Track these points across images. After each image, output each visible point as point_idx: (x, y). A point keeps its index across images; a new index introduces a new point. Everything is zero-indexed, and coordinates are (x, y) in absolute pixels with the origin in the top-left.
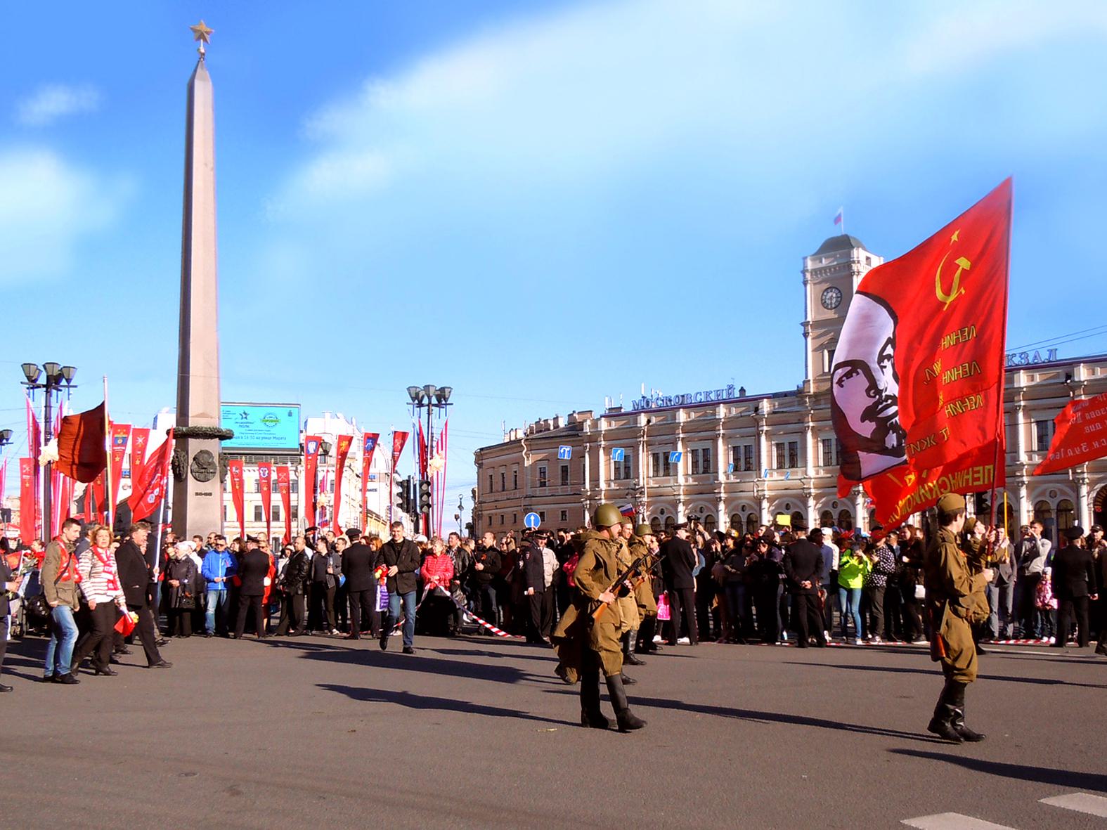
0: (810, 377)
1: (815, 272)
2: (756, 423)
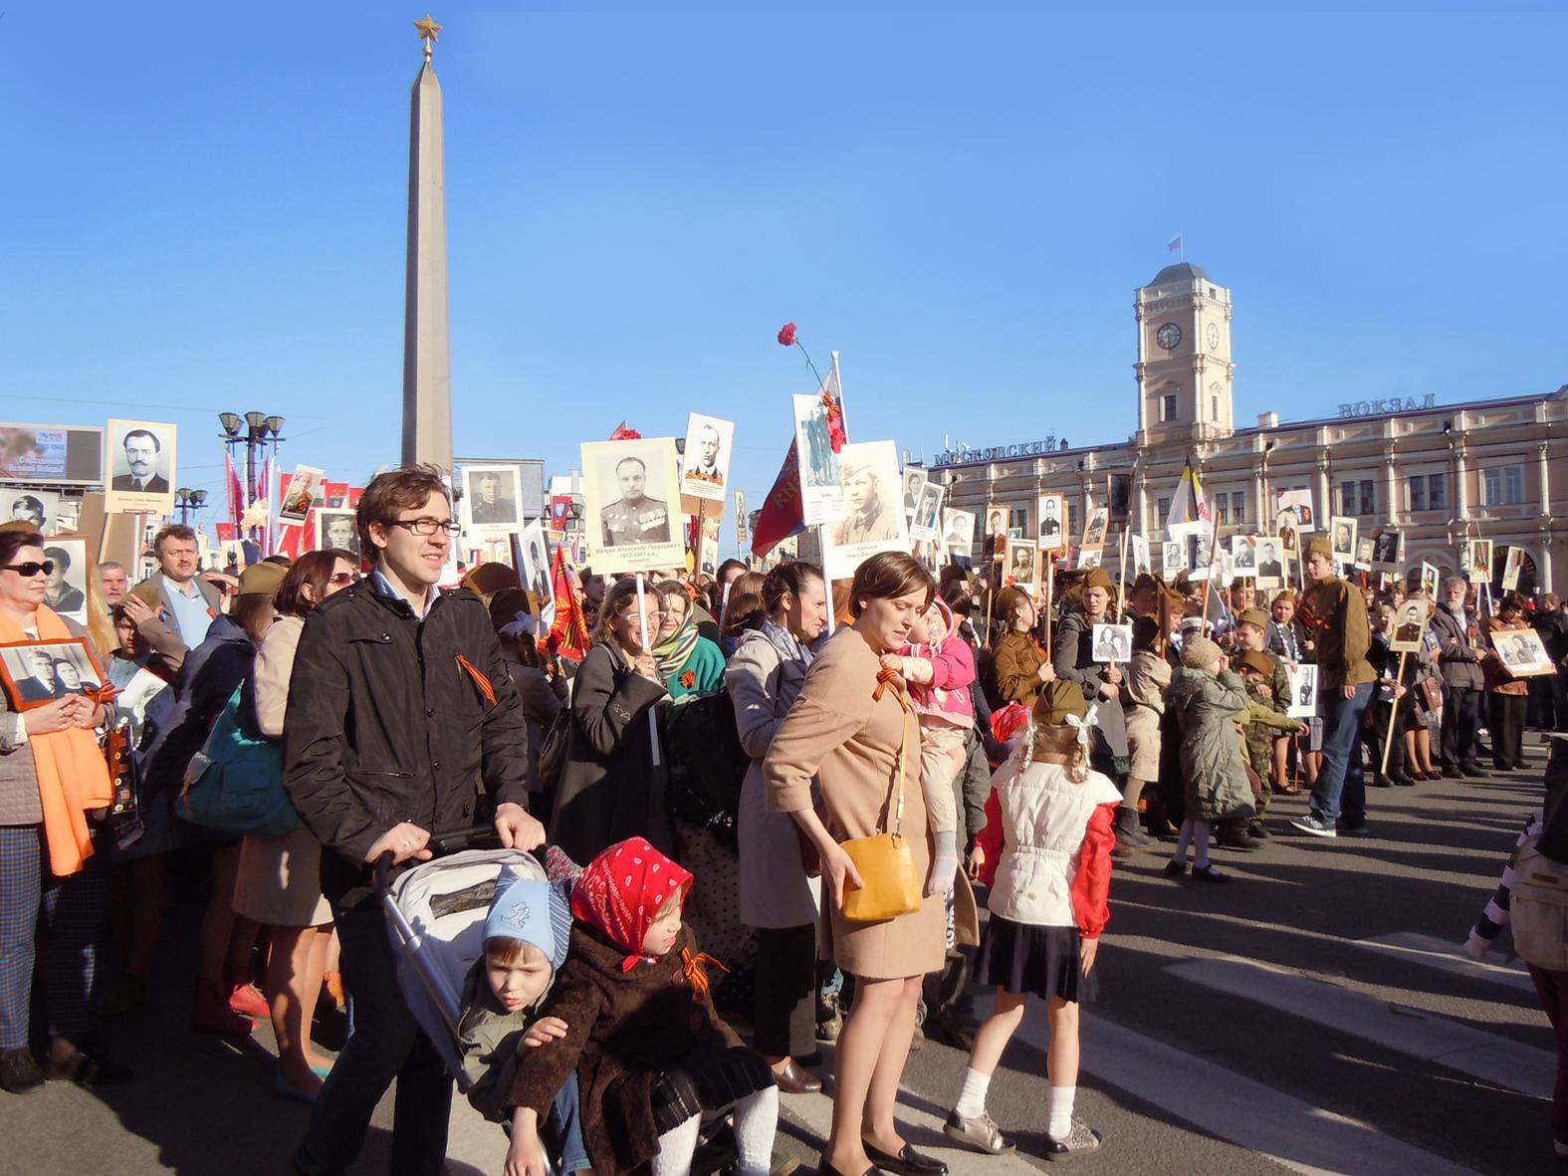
0: (1144, 427)
1: (1149, 306)
2: (1081, 481)
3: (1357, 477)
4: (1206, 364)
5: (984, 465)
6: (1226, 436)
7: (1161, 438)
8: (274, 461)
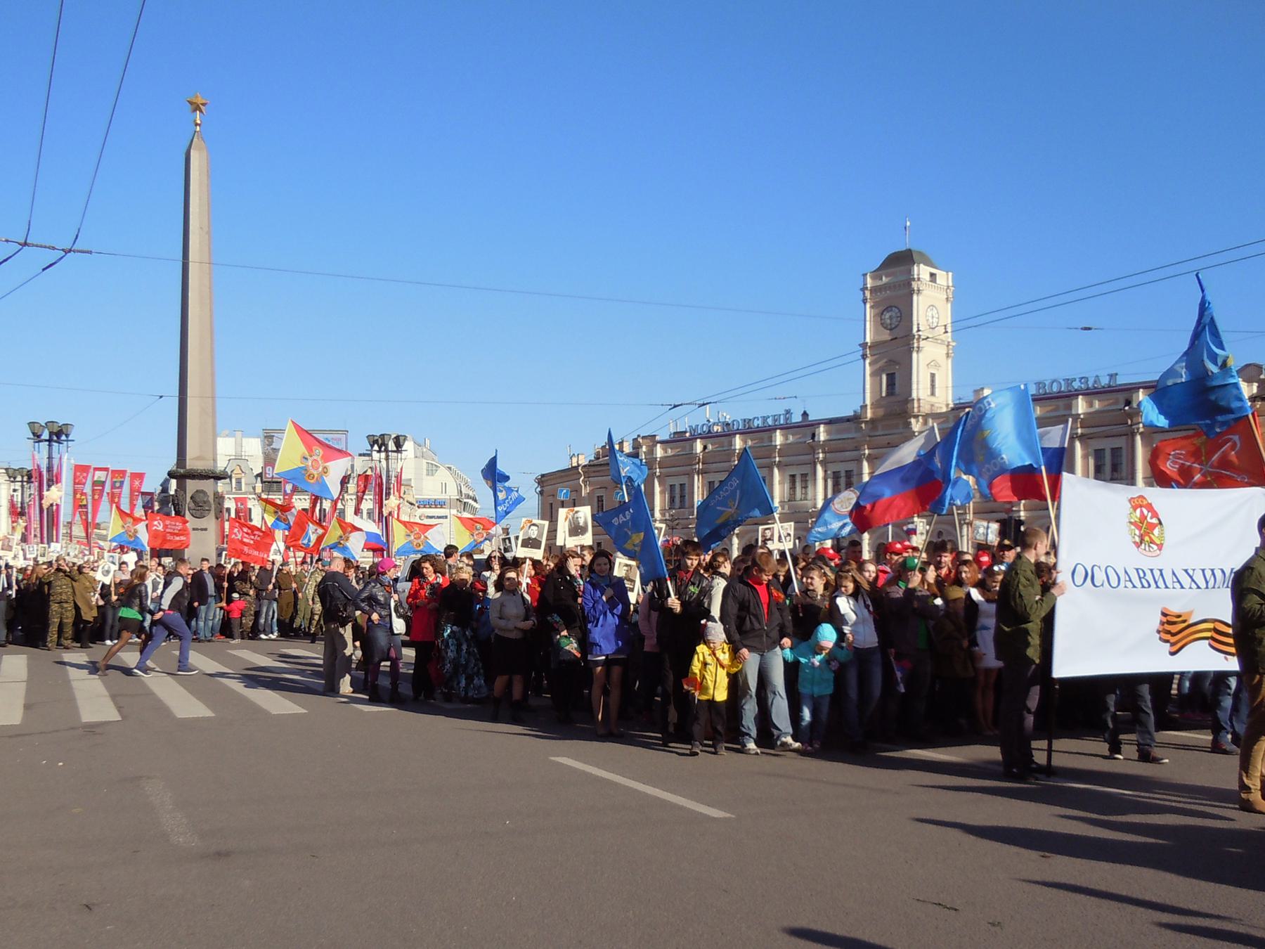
0: (868, 402)
1: (874, 290)
2: (813, 450)
3: (1107, 444)
4: (922, 343)
5: (772, 430)
6: (944, 410)
7: (881, 412)
8: (68, 458)
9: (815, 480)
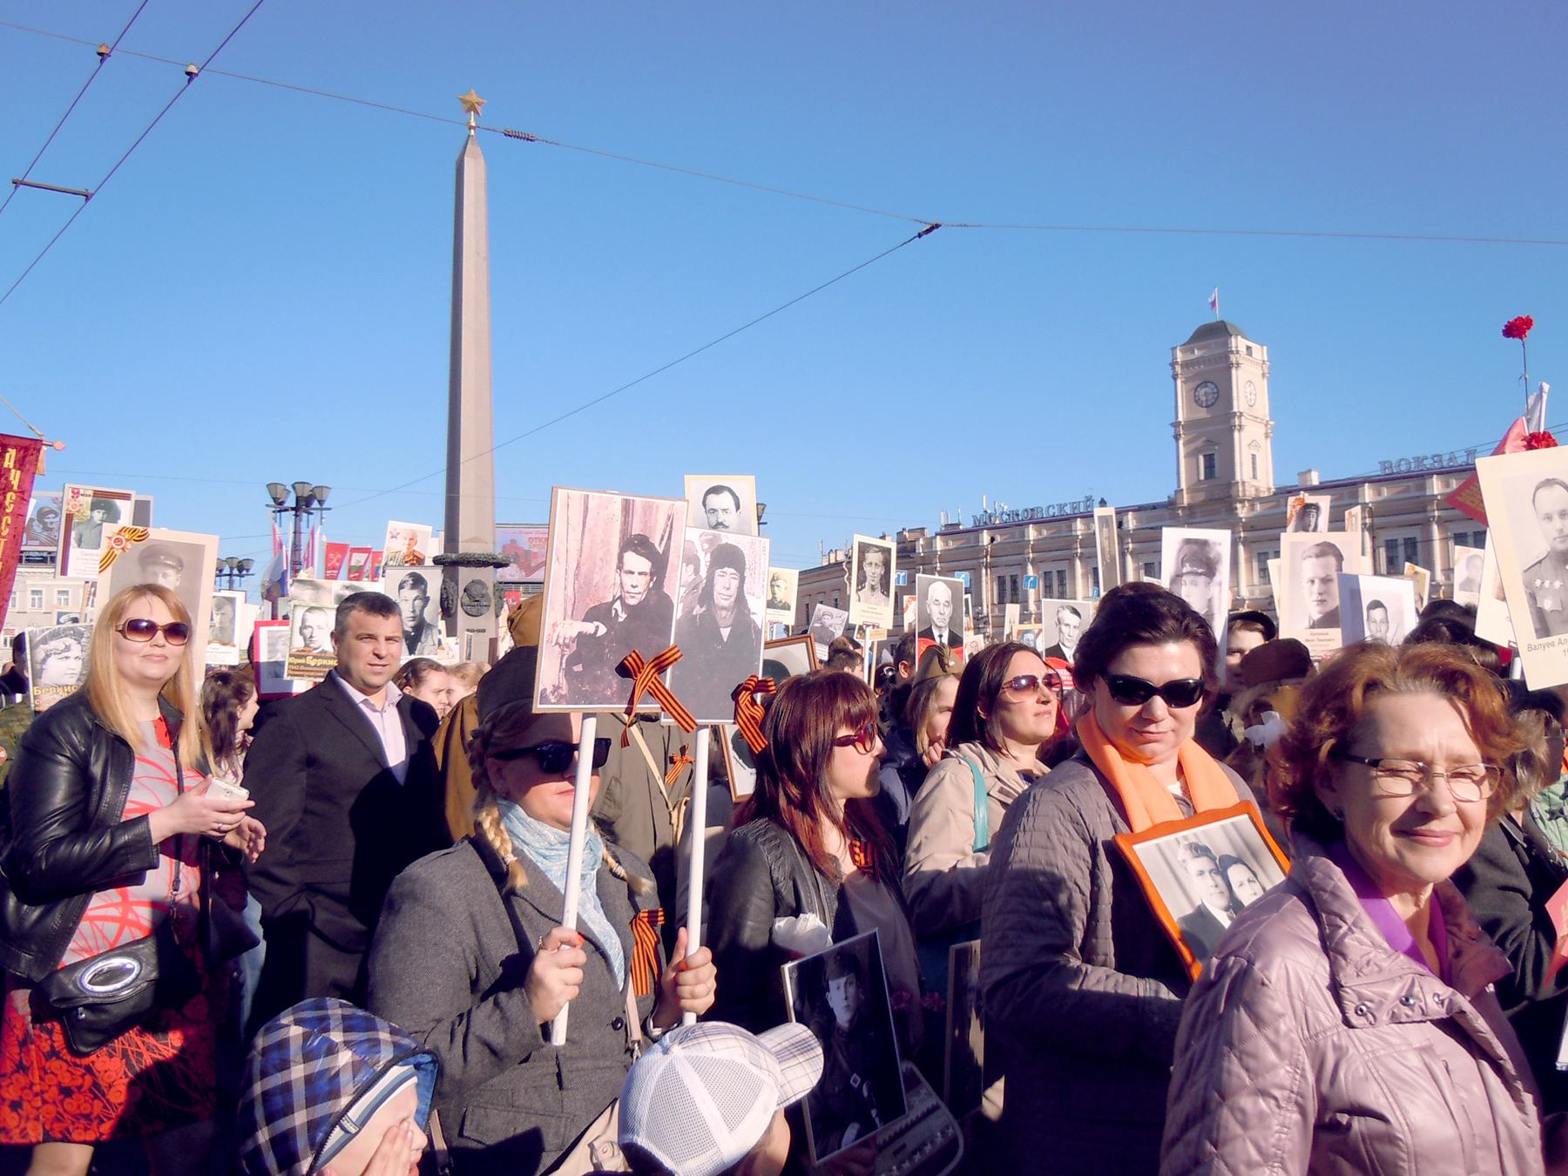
0: (1183, 486)
1: (1186, 365)
5: (1023, 525)
7: (1201, 497)
8: (322, 531)
9: (1073, 578)
